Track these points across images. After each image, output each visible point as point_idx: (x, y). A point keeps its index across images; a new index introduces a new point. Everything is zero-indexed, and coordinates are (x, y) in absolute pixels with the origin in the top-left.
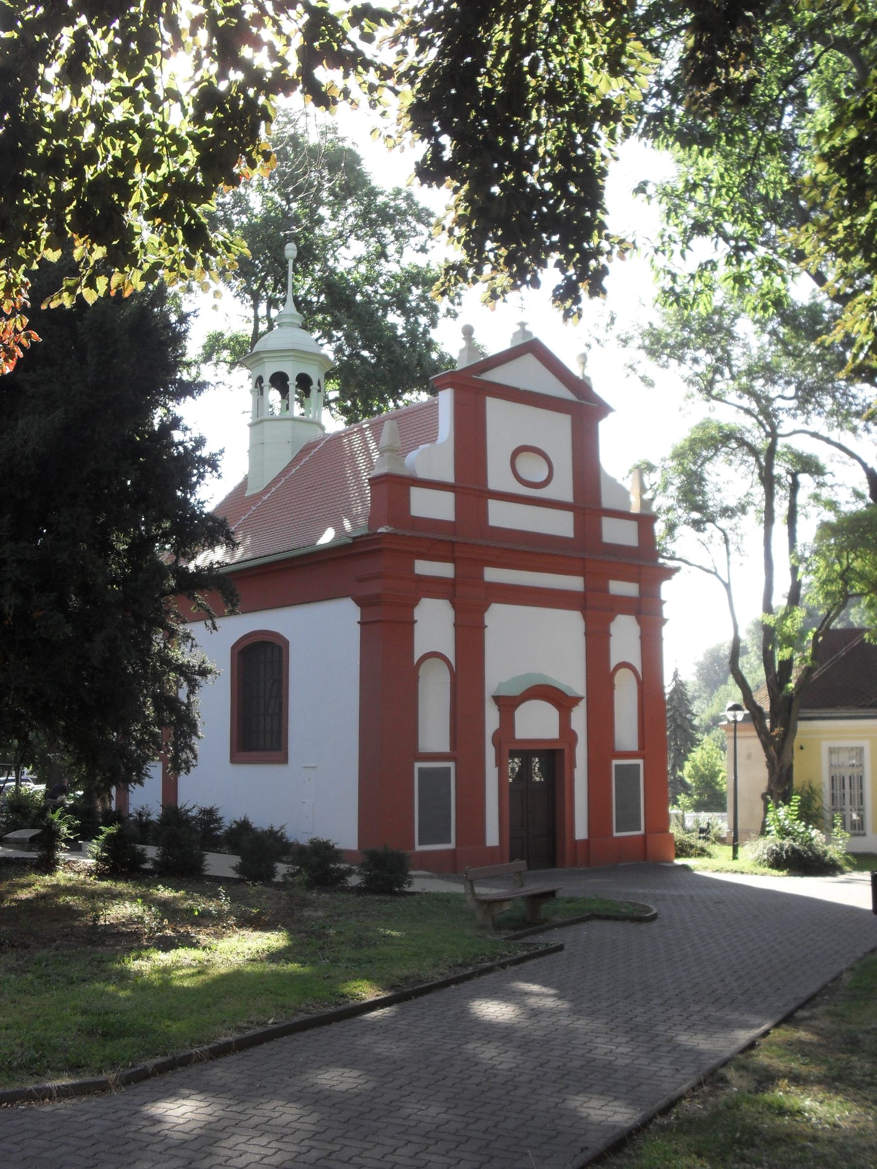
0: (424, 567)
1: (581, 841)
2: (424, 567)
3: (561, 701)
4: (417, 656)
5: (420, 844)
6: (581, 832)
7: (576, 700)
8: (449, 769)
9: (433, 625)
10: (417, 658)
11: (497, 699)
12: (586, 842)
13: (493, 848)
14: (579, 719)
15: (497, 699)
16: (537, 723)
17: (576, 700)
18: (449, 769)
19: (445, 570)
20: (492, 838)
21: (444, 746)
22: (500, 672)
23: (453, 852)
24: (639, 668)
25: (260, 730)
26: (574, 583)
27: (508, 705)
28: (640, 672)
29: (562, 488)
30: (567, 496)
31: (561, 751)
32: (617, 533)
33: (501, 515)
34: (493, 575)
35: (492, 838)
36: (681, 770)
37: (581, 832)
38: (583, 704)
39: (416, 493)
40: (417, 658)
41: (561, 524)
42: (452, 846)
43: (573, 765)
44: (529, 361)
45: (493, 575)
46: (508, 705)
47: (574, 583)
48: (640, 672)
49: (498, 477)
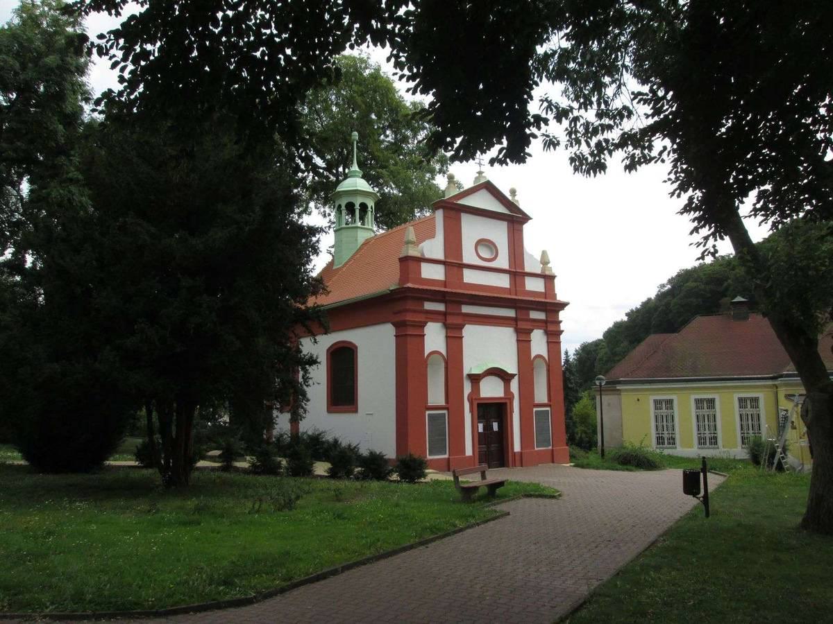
5: (430, 455)
6: (517, 447)
9: (434, 338)
10: (426, 355)
14: (514, 385)
16: (491, 389)
18: (445, 414)
20: (469, 451)
22: (473, 363)
26: (511, 313)
27: (475, 379)
29: (503, 261)
31: (506, 404)
32: (534, 286)
33: (470, 277)
34: (466, 309)
35: (469, 451)
38: (516, 377)
41: (503, 282)
42: (446, 456)
43: (512, 411)
49: (469, 256)
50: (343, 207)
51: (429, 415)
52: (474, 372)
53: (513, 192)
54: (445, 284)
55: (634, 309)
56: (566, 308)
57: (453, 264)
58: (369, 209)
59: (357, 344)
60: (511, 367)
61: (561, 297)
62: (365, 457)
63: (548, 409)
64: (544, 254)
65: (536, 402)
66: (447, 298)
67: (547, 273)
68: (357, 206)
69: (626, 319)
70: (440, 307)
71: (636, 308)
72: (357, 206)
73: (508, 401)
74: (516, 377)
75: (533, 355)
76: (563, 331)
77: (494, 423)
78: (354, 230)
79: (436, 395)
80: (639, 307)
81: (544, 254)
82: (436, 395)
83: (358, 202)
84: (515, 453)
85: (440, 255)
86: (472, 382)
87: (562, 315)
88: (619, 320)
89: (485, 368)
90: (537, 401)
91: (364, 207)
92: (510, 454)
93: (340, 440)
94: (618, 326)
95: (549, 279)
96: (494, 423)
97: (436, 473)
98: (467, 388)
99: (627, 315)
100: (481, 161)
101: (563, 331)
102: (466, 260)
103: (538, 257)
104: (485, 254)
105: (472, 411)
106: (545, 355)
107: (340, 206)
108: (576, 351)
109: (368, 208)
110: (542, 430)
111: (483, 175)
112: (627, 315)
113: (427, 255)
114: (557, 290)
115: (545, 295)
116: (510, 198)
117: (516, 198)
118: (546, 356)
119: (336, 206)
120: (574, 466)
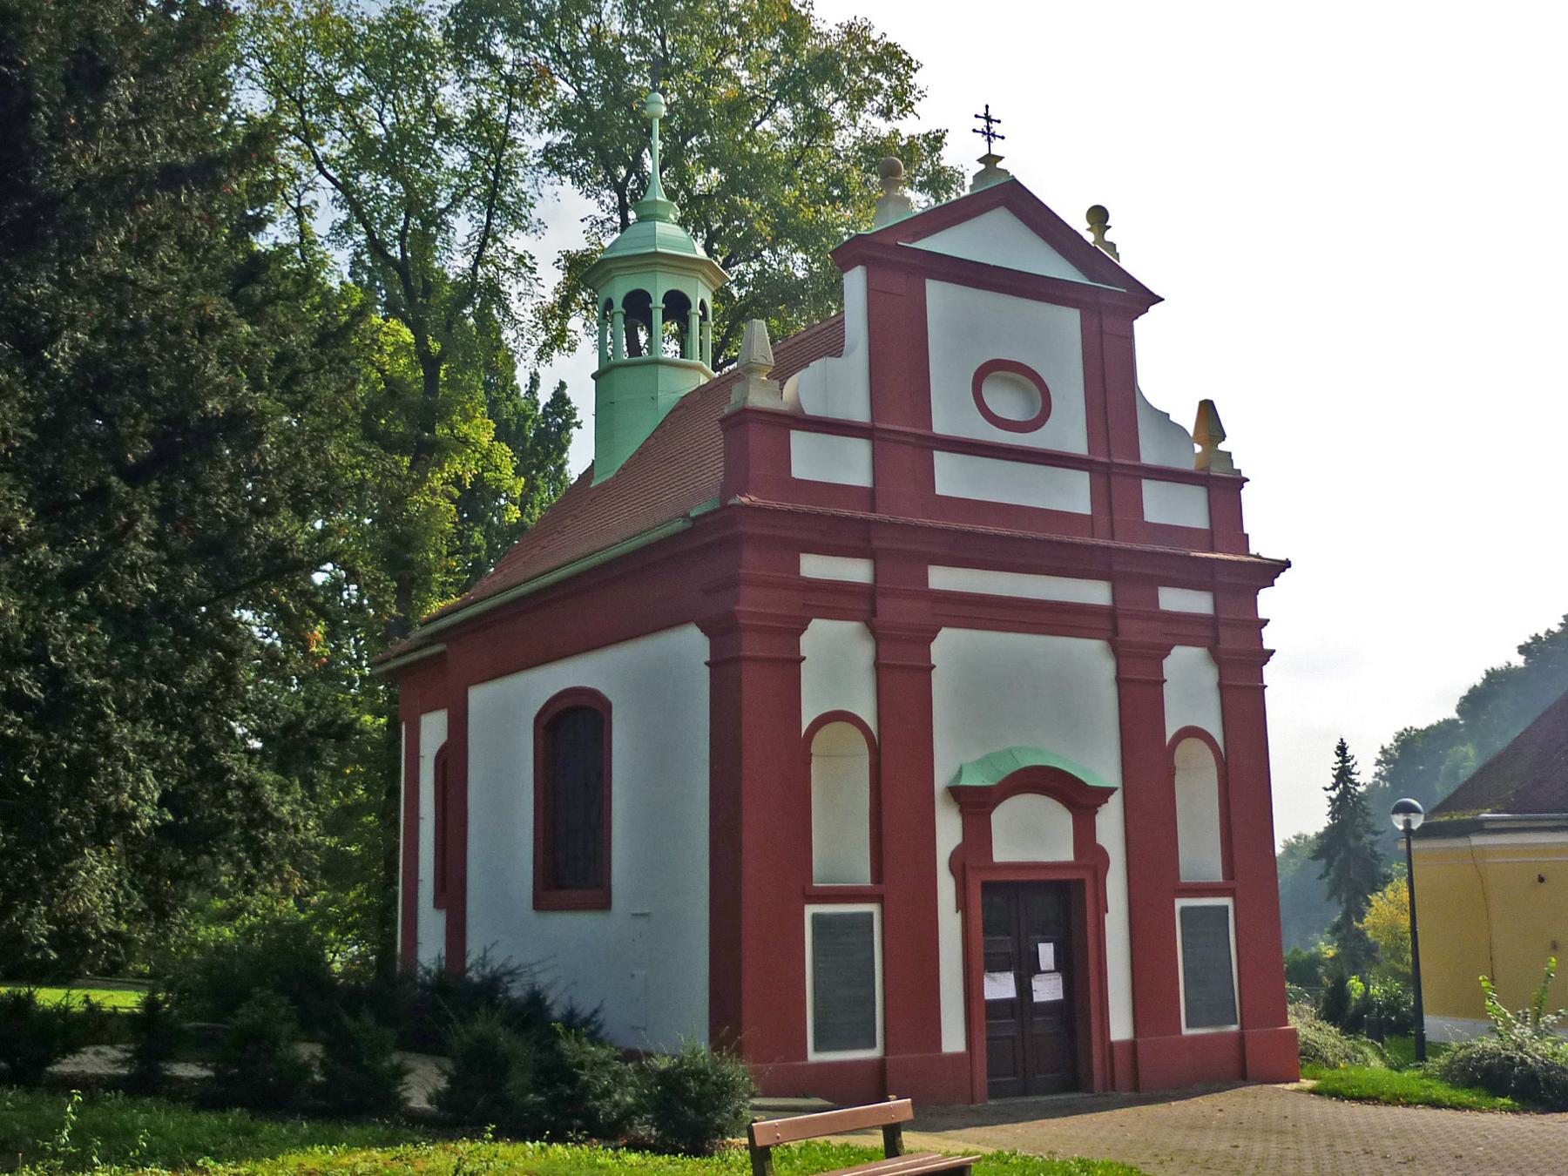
0: (814, 567)
1: (1121, 1044)
2: (814, 567)
3: (1080, 800)
4: (1170, 733)
5: (817, 1049)
6: (1120, 1028)
7: (1104, 794)
8: (871, 915)
9: (835, 667)
11: (959, 794)
12: (1132, 1046)
13: (955, 1057)
14: (1110, 826)
15: (959, 794)
16: (1031, 836)
17: (1104, 794)
18: (871, 915)
19: (857, 571)
21: (861, 873)
23: (880, 1064)
24: (871, 722)
25: (572, 862)
26: (1096, 593)
27: (976, 805)
28: (875, 732)
29: (1068, 430)
30: (1076, 442)
31: (1080, 883)
32: (1172, 508)
33: (952, 477)
34: (942, 578)
36: (1360, 921)
37: (1120, 1028)
38: (1116, 801)
39: (799, 441)
40: (1169, 736)
41: (1072, 494)
42: (875, 1053)
43: (1102, 907)
44: (1000, 221)
45: (942, 578)
46: (976, 805)
47: (1096, 593)
48: (875, 732)
49: (950, 413)
50: (618, 305)
51: (815, 917)
52: (972, 780)
53: (1099, 216)
54: (868, 497)
55: (1542, 634)
56: (1283, 579)
57: (901, 432)
58: (696, 309)
59: (610, 698)
60: (1101, 766)
61: (1263, 544)
62: (77, 1014)
63: (1227, 901)
64: (1207, 409)
65: (1183, 880)
66: (876, 544)
67: (1216, 471)
68: (658, 303)
69: (1519, 661)
70: (857, 571)
71: (1549, 631)
72: (658, 303)
73: (1087, 877)
74: (1116, 801)
75: (1171, 731)
76: (1272, 652)
77: (1041, 946)
78: (653, 367)
79: (840, 841)
80: (1556, 629)
81: (1207, 409)
82: (840, 841)
83: (659, 287)
84: (1111, 1045)
85: (858, 410)
86: (962, 812)
87: (1267, 602)
88: (1499, 664)
89: (1008, 768)
90: (1187, 874)
91: (677, 306)
92: (1096, 1050)
93: (551, 997)
94: (1496, 680)
95: (1225, 488)
96: (1041, 946)
97: (1513, 1111)
98: (949, 831)
99: (1522, 649)
100: (994, 125)
101: (1272, 652)
102: (941, 425)
103: (1187, 419)
104: (1006, 401)
105: (962, 904)
106: (1213, 726)
107: (609, 304)
108: (1384, 751)
109: (689, 306)
110: (1205, 973)
111: (1000, 165)
112: (1522, 649)
113: (811, 408)
114: (1252, 523)
115: (1208, 539)
116: (1090, 237)
117: (1109, 236)
118: (1215, 730)
119: (602, 302)
120: (649, 1055)
